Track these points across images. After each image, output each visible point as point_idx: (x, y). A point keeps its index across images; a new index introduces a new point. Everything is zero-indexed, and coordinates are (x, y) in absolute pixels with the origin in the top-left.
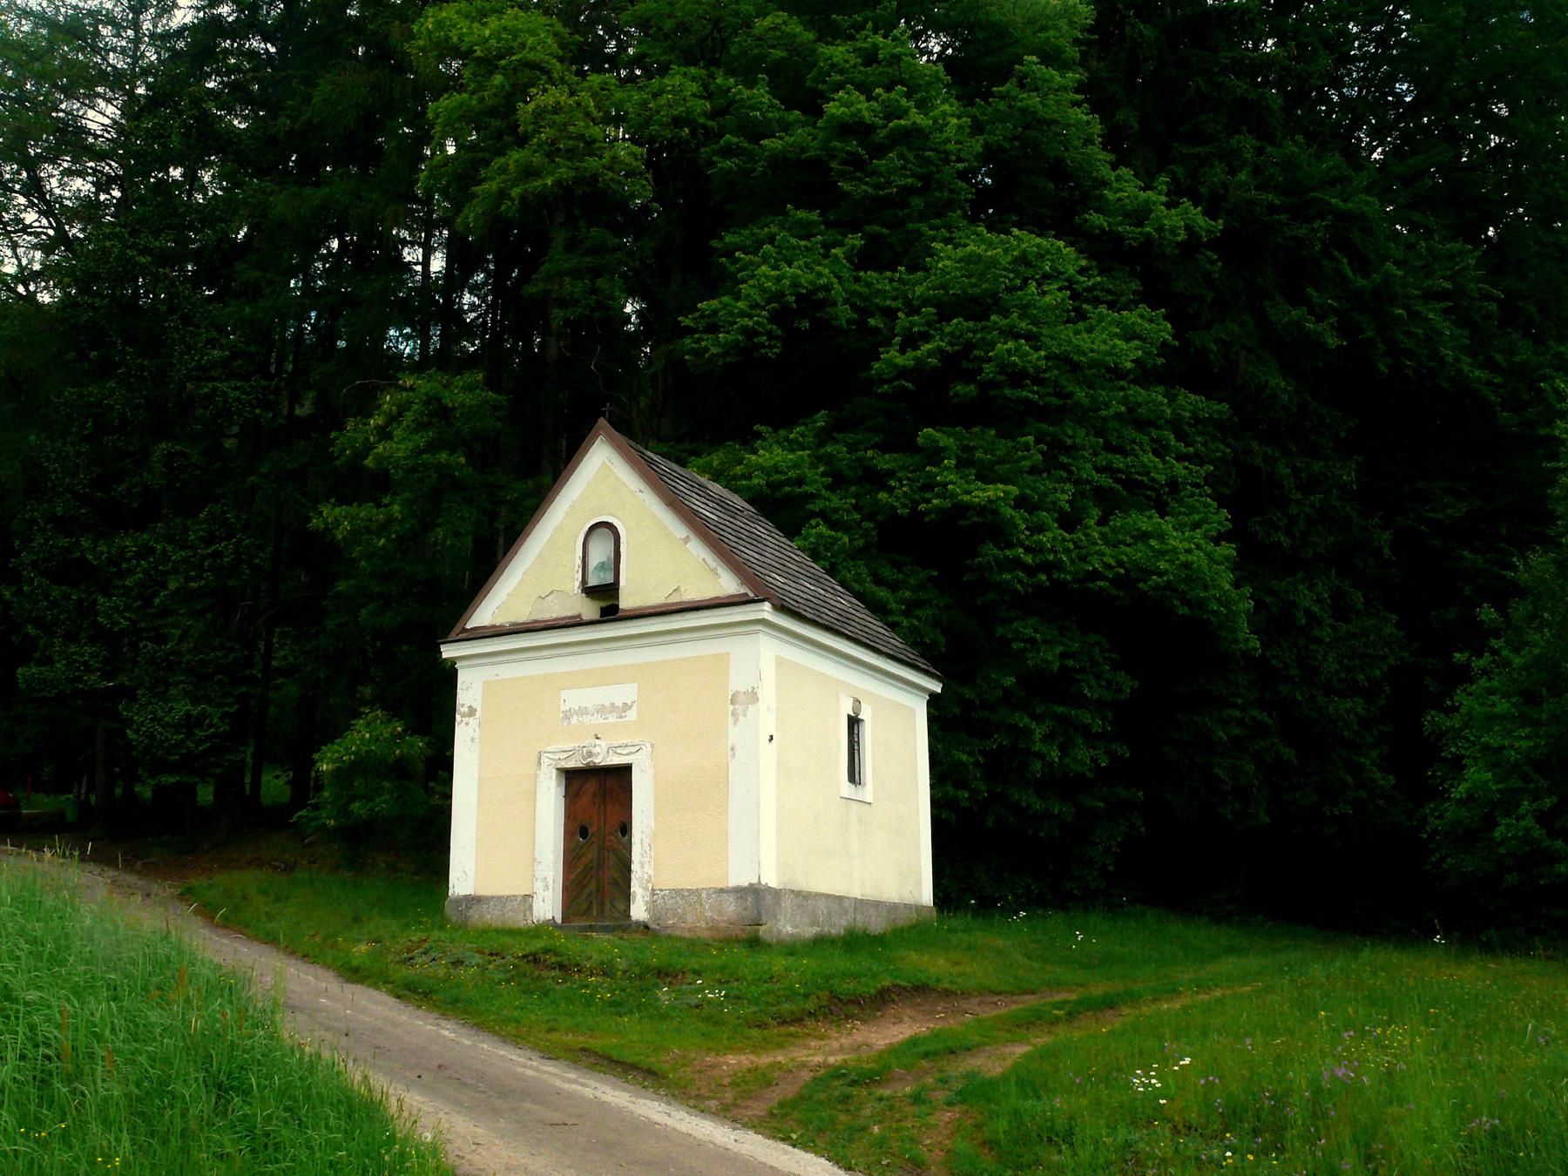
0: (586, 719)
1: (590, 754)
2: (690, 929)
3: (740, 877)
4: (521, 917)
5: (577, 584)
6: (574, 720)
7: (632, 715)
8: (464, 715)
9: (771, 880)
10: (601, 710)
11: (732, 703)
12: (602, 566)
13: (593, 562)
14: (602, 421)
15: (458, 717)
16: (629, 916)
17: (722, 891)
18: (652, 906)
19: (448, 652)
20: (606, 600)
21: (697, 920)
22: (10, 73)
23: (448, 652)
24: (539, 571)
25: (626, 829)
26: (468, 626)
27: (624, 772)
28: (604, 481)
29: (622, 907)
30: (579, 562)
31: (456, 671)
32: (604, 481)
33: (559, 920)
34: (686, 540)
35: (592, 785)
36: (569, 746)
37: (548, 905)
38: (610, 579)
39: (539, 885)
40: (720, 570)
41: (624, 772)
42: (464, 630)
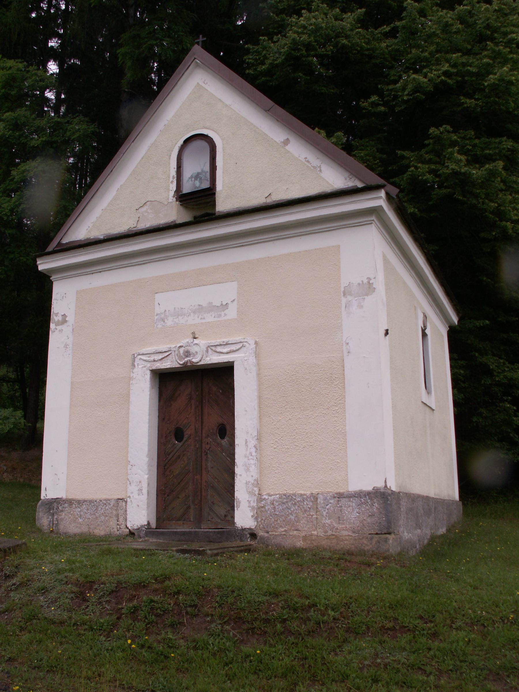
0: (182, 320)
1: (187, 353)
2: (305, 538)
3: (363, 479)
4: (113, 523)
5: (172, 193)
6: (169, 322)
7: (232, 313)
8: (58, 324)
9: (393, 486)
10: (200, 310)
11: (344, 295)
12: (197, 176)
13: (188, 172)
14: (197, 49)
15: (52, 326)
16: (234, 523)
17: (340, 496)
18: (259, 512)
19: (44, 265)
20: (199, 205)
21: (298, 533)
22: (34, 15)
23: (44, 265)
24: (138, 185)
25: (226, 430)
26: (64, 241)
27: (224, 373)
28: (203, 101)
29: (221, 511)
30: (173, 172)
31: (51, 283)
32: (203, 101)
33: (153, 525)
34: (286, 142)
35: (187, 390)
36: (164, 347)
37: (140, 512)
38: (206, 185)
39: (133, 489)
40: (324, 168)
41: (224, 373)
42: (59, 244)
